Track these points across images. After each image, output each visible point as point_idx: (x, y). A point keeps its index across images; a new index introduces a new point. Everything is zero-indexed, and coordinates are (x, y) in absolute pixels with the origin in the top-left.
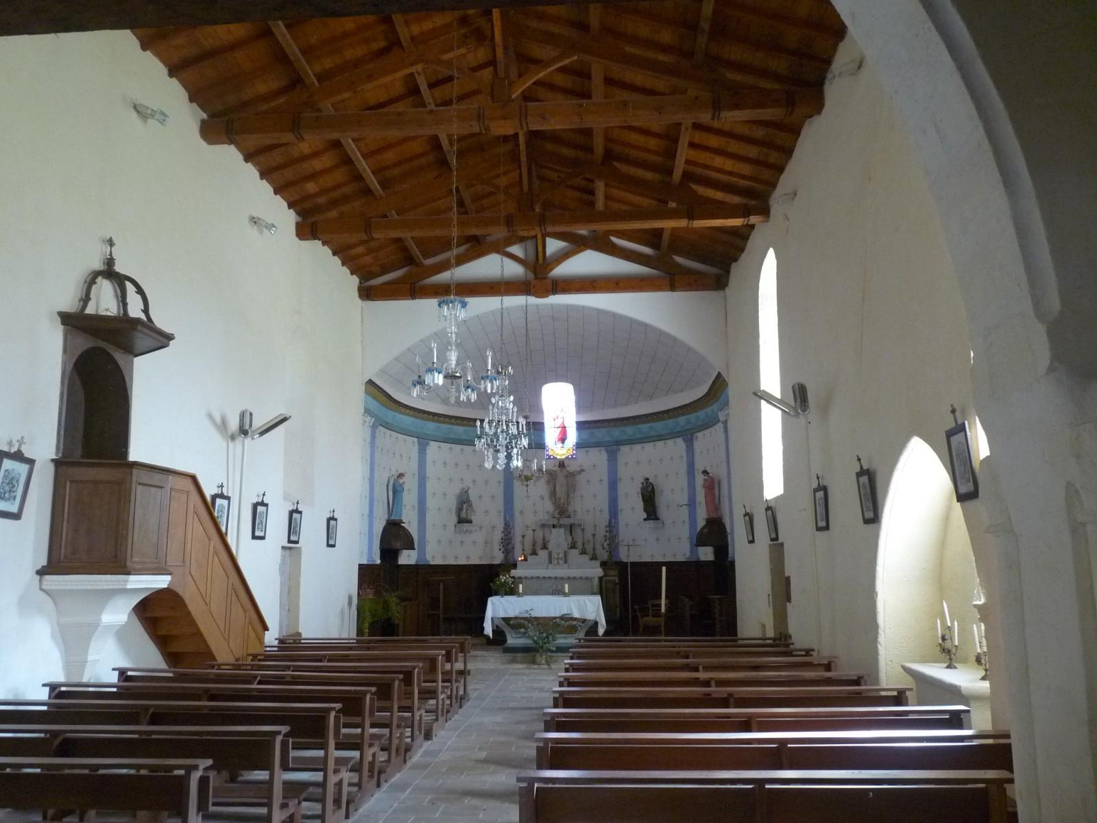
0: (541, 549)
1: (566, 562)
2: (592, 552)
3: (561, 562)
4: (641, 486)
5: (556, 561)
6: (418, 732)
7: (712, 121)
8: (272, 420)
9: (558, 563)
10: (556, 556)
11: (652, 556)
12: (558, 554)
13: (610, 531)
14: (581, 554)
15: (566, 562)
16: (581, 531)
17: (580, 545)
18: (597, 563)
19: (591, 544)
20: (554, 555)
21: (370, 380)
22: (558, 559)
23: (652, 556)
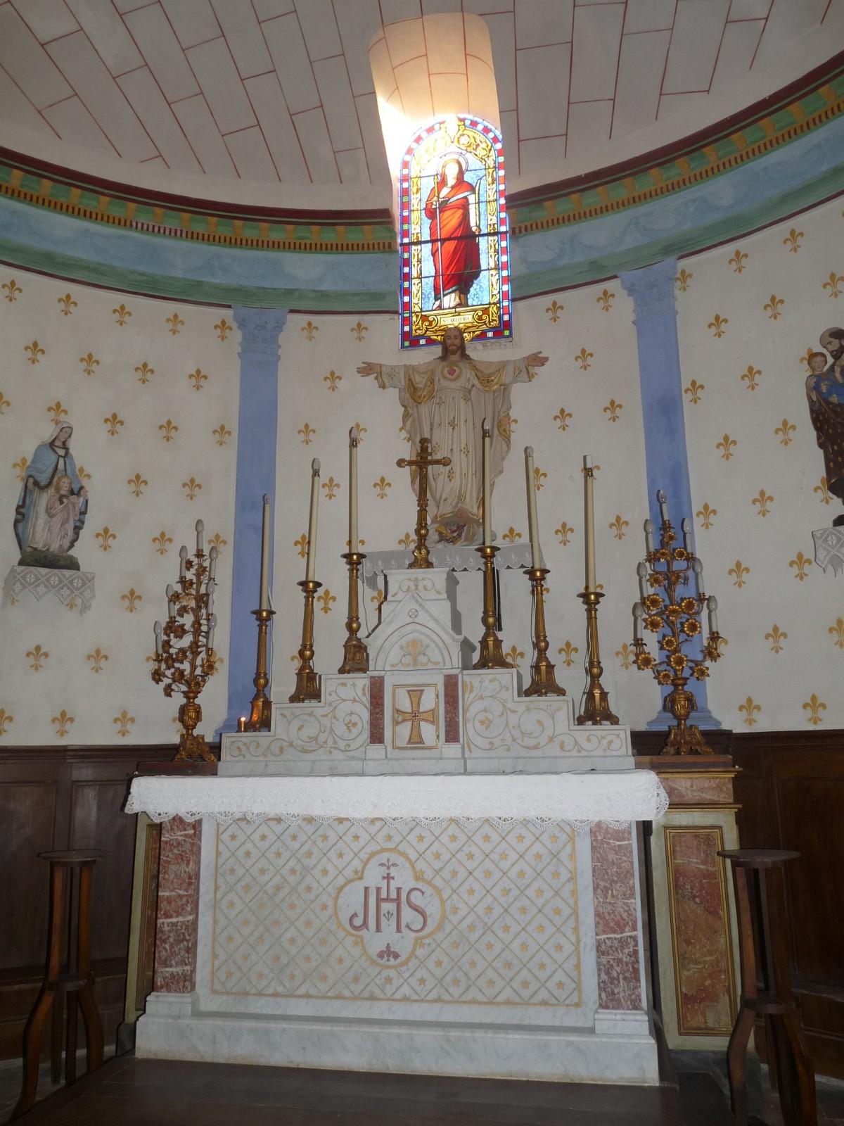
0: (294, 699)
1: (452, 734)
2: (531, 655)
3: (428, 731)
4: (804, 372)
5: (405, 730)
6: (49, 1079)
7: (281, 850)
8: (499, 598)
9: (416, 741)
10: (405, 704)
11: (814, 704)
12: (416, 693)
13: (670, 580)
14: (581, 721)
15: (452, 734)
16: (526, 583)
17: (572, 678)
18: (617, 739)
19: (581, 658)
20: (401, 700)
21: (758, 870)
22: (415, 716)
23: (814, 704)
